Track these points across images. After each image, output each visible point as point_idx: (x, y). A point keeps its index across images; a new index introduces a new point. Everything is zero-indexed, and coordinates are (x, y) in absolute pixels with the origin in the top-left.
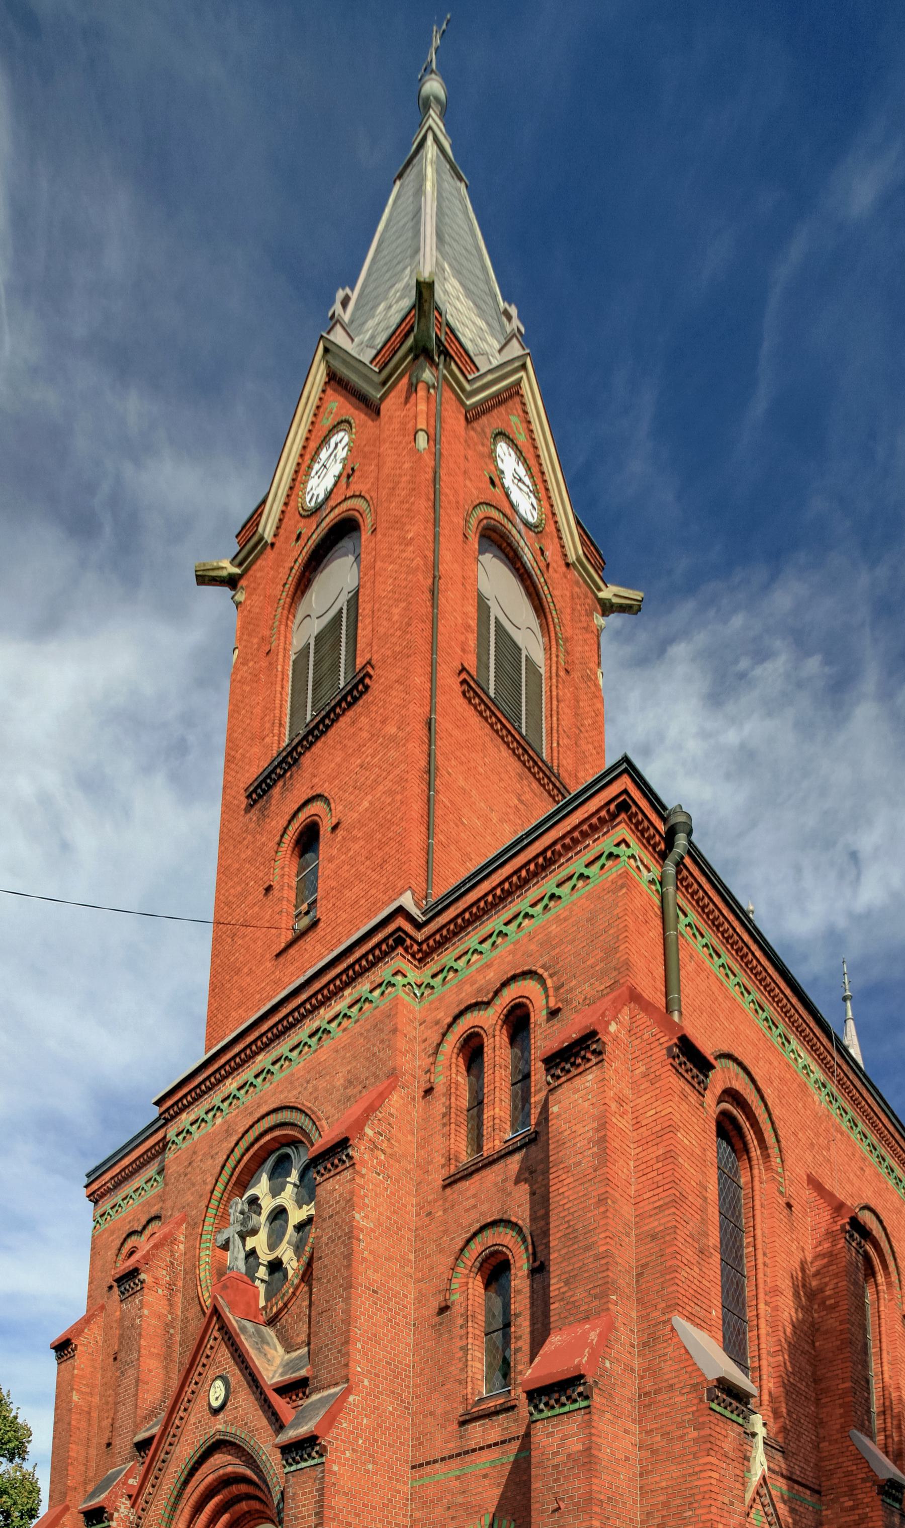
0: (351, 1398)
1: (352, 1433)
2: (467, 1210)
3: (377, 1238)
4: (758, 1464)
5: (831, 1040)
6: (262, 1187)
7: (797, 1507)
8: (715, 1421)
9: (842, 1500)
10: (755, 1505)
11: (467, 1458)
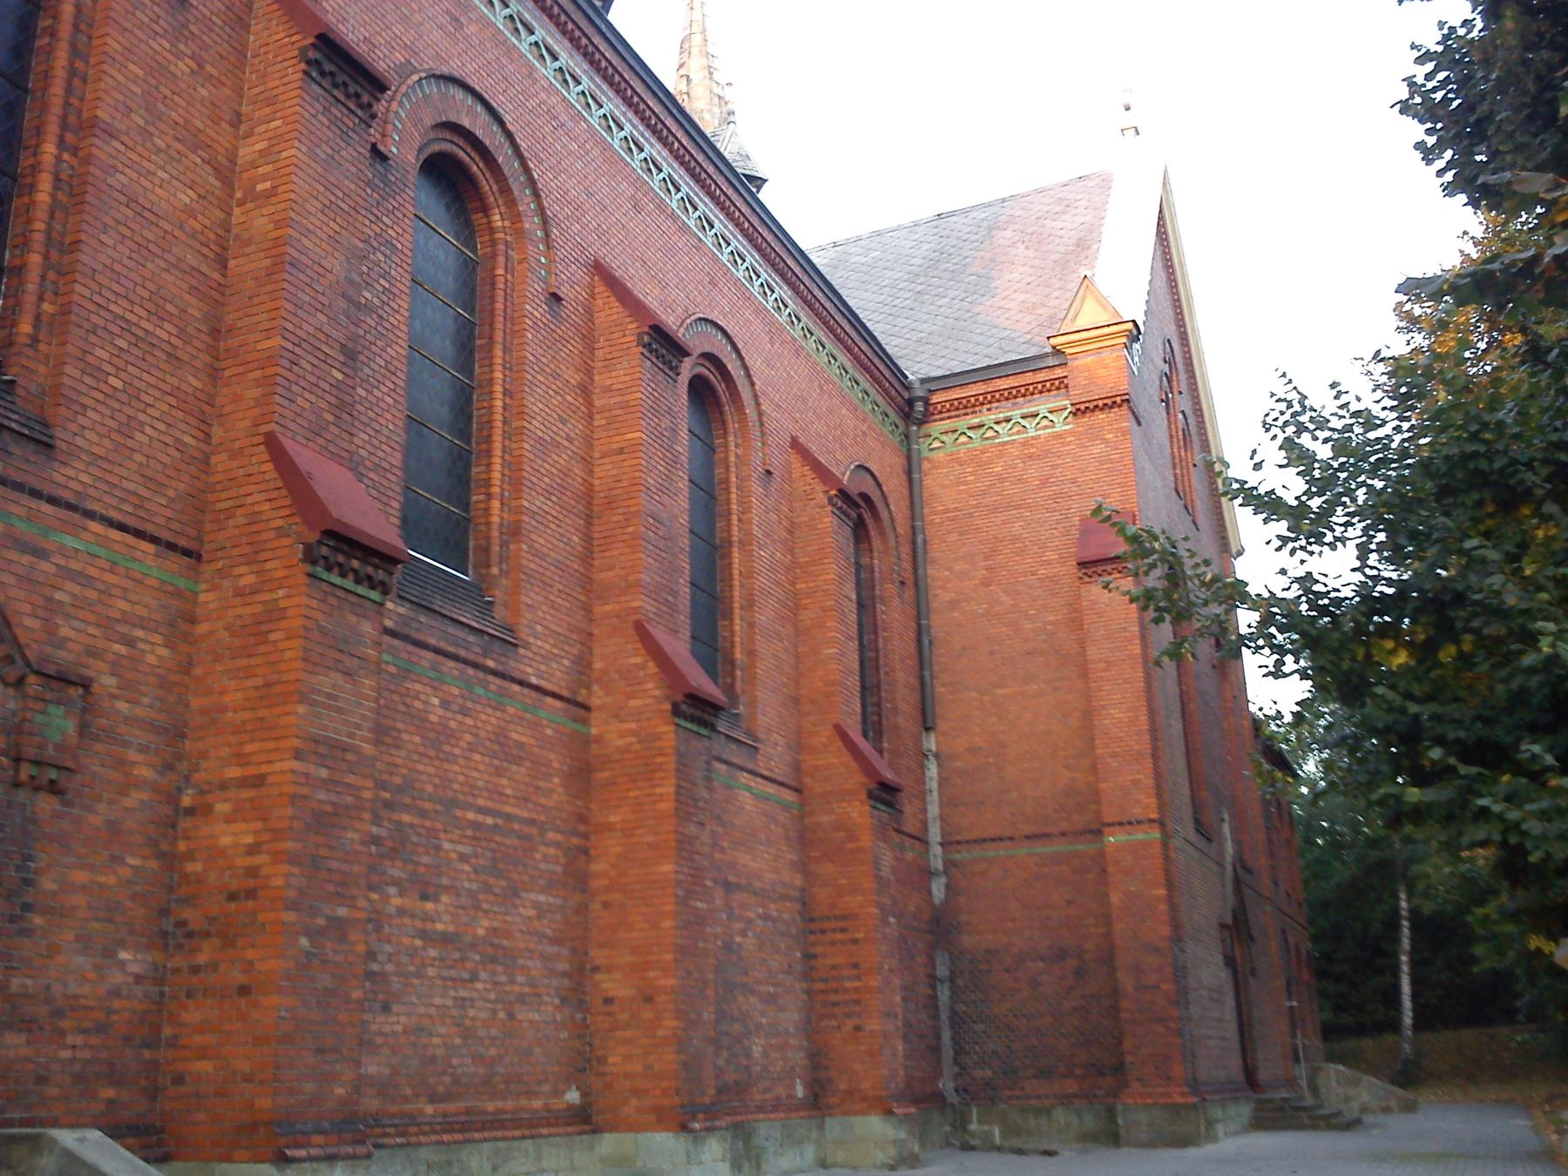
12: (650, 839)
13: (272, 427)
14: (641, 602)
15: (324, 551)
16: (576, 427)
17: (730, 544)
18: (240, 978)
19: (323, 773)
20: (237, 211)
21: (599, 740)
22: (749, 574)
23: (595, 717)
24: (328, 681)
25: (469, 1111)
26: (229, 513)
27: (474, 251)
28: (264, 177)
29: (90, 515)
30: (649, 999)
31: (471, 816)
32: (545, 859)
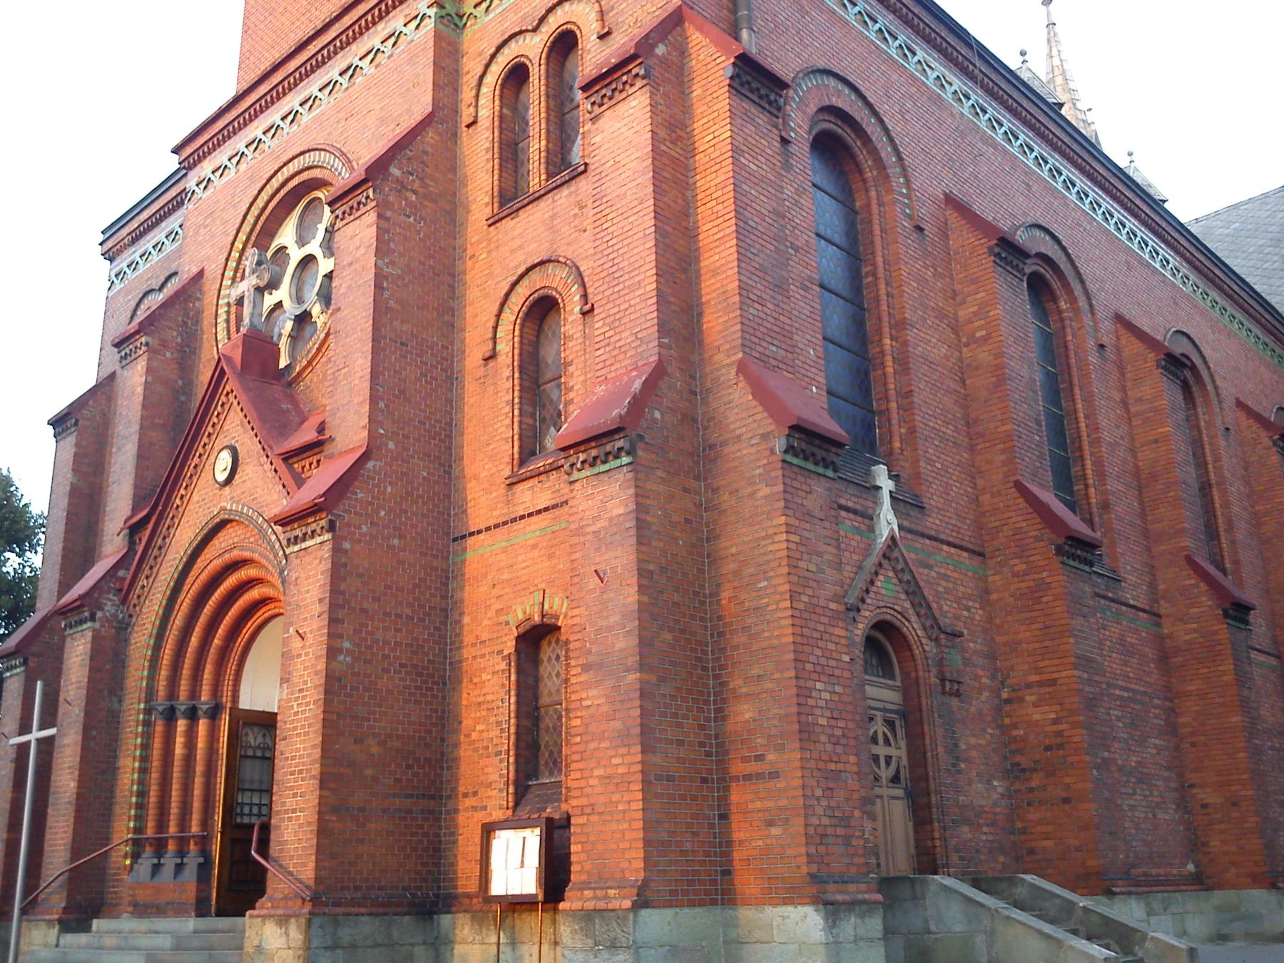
0: (370, 465)
1: (371, 503)
2: (512, 252)
3: (407, 285)
4: (883, 522)
5: (971, 47)
6: (286, 236)
7: (949, 573)
8: (793, 475)
9: (1012, 562)
10: (882, 571)
11: (516, 526)
12: (1221, 700)
13: (1018, 477)
14: (1188, 542)
15: (1067, 548)
16: (1124, 428)
17: (1210, 485)
18: (1064, 794)
19: (1085, 675)
20: (965, 350)
21: (1170, 636)
22: (1226, 505)
23: (1164, 620)
24: (1078, 622)
25: (1145, 874)
26: (999, 529)
27: (1049, 326)
28: (980, 328)
29: (943, 542)
30: (1235, 804)
31: (1117, 692)
32: (1156, 717)
